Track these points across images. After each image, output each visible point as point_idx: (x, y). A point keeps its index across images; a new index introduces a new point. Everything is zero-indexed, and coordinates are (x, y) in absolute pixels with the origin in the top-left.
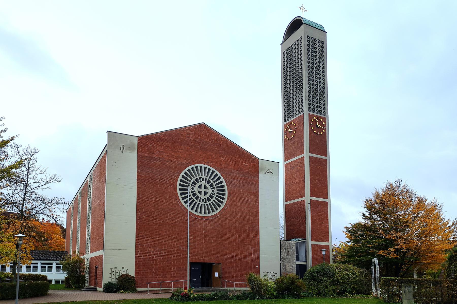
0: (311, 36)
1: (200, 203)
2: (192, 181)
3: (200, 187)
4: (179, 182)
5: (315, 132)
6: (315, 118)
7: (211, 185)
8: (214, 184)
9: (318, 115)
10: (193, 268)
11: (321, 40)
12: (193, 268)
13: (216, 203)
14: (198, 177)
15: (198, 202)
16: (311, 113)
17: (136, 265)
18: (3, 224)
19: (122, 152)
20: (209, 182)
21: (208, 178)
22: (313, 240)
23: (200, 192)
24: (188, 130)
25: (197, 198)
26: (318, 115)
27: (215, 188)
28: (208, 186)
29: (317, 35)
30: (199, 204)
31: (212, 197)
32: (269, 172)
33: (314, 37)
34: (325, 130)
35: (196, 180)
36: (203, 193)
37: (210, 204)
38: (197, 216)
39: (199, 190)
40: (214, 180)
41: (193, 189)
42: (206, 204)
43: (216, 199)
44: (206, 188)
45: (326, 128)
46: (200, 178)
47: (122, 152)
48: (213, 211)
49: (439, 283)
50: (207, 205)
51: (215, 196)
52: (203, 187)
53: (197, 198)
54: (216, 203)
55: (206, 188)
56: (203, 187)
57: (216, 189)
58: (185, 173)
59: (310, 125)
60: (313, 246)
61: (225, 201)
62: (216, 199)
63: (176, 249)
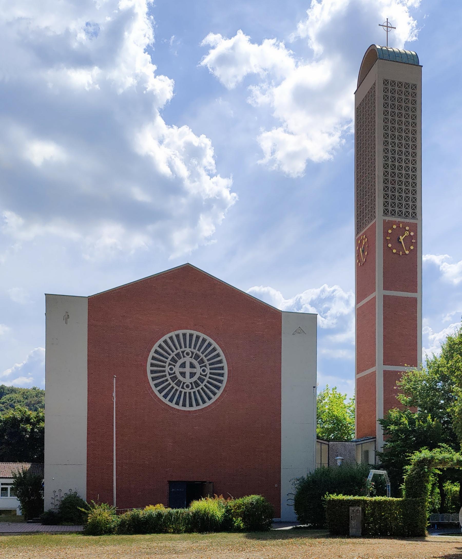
0: (390, 78)
1: (183, 391)
2: (170, 357)
3: (183, 365)
4: (150, 361)
5: (390, 245)
6: (395, 227)
7: (202, 362)
8: (205, 359)
9: (403, 220)
10: (173, 490)
11: (411, 82)
12: (173, 490)
13: (163, 382)
14: (179, 350)
16: (388, 218)
19: (66, 323)
20: (197, 357)
23: (183, 374)
26: (403, 220)
27: (208, 365)
28: (195, 363)
29: (400, 74)
32: (299, 331)
33: (397, 80)
34: (416, 247)
35: (177, 355)
36: (188, 375)
37: (198, 391)
39: (182, 370)
40: (178, 347)
41: (171, 369)
42: (192, 391)
44: (192, 366)
45: (416, 243)
46: (183, 352)
48: (204, 402)
49: (263, 75)
50: (194, 392)
51: (207, 379)
52: (188, 365)
54: (163, 382)
56: (188, 365)
57: (209, 367)
58: (160, 346)
59: (386, 242)
62: (208, 382)
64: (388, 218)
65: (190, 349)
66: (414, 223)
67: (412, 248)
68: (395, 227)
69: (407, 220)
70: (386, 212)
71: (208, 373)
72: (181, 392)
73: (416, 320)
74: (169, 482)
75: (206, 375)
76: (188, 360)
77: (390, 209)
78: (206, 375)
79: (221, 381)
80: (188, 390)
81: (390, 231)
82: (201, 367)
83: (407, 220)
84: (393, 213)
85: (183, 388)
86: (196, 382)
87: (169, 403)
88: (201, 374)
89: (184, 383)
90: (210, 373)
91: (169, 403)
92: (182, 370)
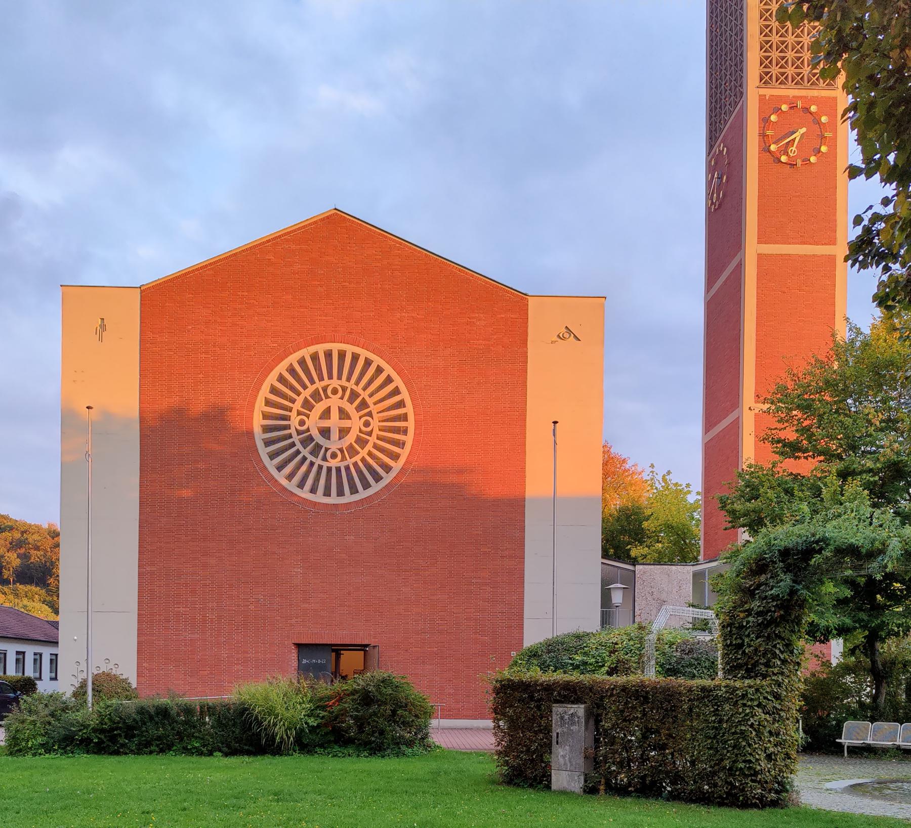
9: (803, 93)
10: (304, 661)
12: (304, 661)
13: (292, 388)
15: (318, 461)
16: (768, 92)
17: (139, 652)
18: (728, 752)
19: (101, 339)
21: (351, 385)
22: (762, 239)
24: (287, 240)
25: (316, 451)
26: (803, 93)
28: (350, 409)
30: (320, 467)
31: (362, 442)
38: (315, 504)
39: (346, 423)
43: (375, 446)
47: (101, 339)
53: (316, 451)
54: (292, 388)
55: (344, 415)
60: (761, 257)
61: (306, 353)
63: (252, 607)
64: (768, 92)
65: (339, 382)
66: (829, 98)
67: (824, 149)
68: (784, 107)
69: (815, 93)
70: (765, 79)
71: (329, 465)
72: (320, 467)
73: (834, 304)
74: (299, 646)
75: (327, 461)
76: (334, 402)
77: (775, 70)
78: (327, 461)
79: (302, 362)
80: (333, 463)
81: (773, 118)
82: (327, 397)
83: (815, 93)
84: (783, 80)
85: (324, 459)
86: (351, 447)
87: (408, 402)
88: (361, 431)
89: (327, 450)
90: (340, 378)
91: (408, 402)
92: (346, 423)
